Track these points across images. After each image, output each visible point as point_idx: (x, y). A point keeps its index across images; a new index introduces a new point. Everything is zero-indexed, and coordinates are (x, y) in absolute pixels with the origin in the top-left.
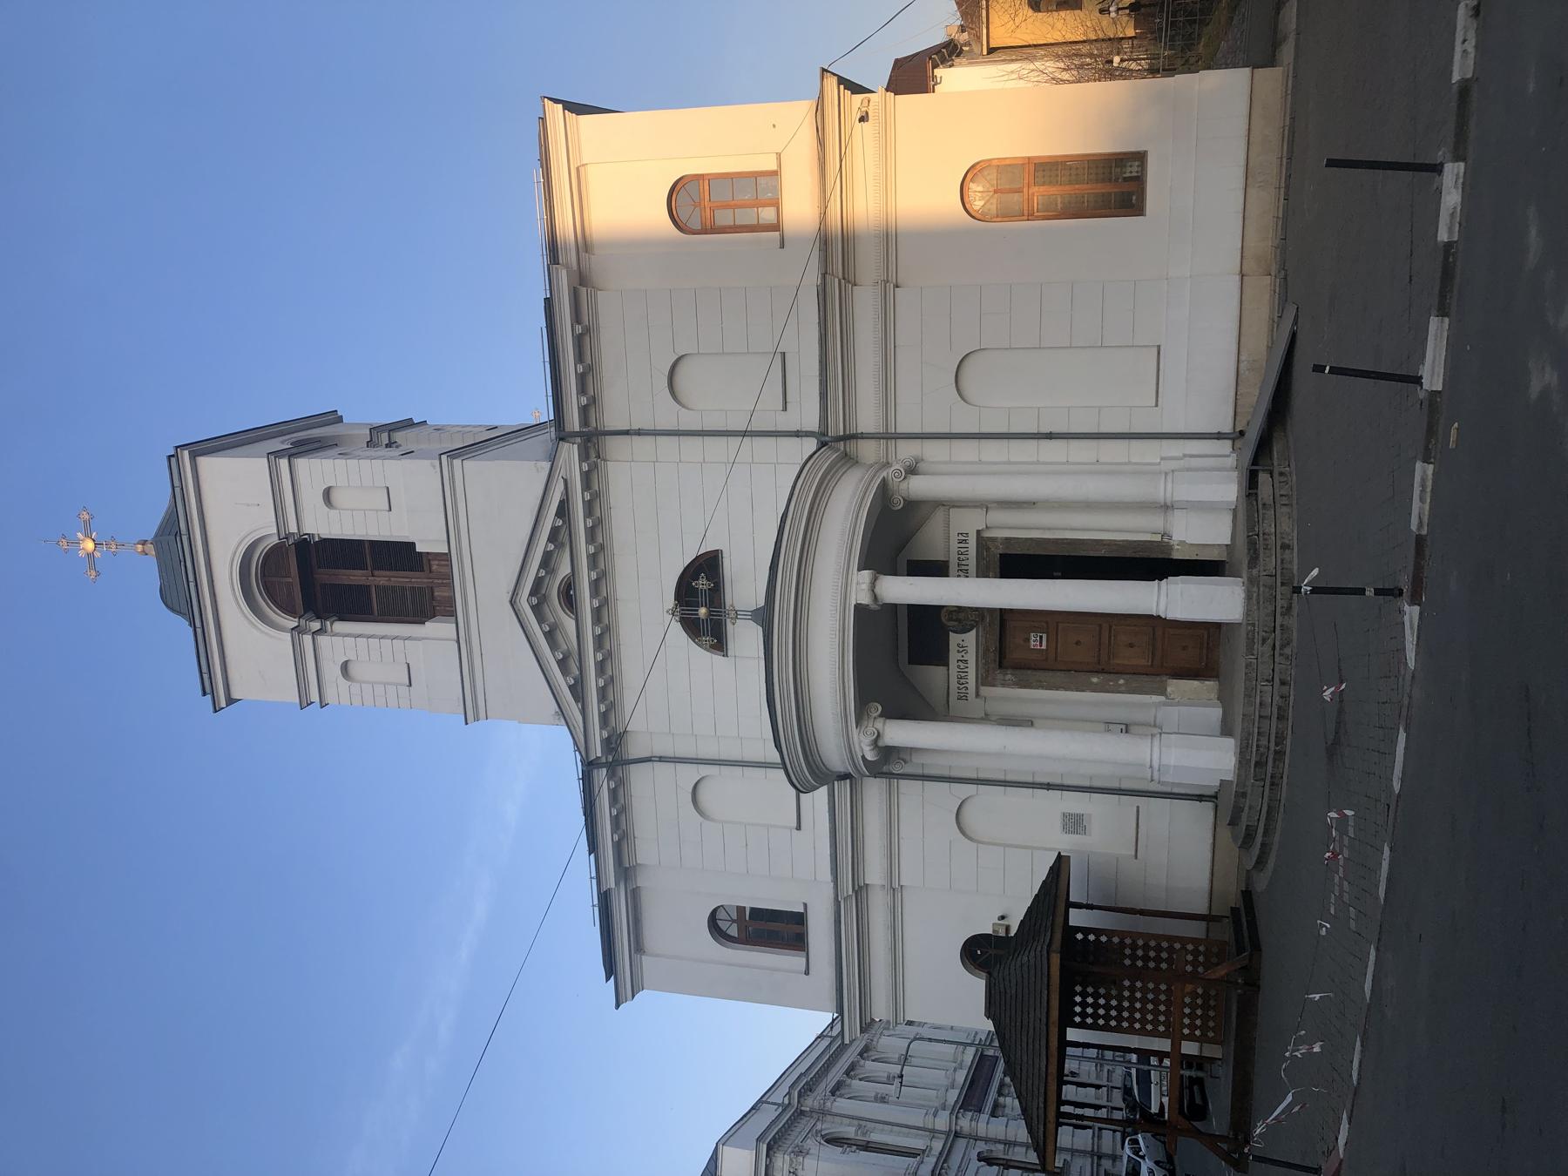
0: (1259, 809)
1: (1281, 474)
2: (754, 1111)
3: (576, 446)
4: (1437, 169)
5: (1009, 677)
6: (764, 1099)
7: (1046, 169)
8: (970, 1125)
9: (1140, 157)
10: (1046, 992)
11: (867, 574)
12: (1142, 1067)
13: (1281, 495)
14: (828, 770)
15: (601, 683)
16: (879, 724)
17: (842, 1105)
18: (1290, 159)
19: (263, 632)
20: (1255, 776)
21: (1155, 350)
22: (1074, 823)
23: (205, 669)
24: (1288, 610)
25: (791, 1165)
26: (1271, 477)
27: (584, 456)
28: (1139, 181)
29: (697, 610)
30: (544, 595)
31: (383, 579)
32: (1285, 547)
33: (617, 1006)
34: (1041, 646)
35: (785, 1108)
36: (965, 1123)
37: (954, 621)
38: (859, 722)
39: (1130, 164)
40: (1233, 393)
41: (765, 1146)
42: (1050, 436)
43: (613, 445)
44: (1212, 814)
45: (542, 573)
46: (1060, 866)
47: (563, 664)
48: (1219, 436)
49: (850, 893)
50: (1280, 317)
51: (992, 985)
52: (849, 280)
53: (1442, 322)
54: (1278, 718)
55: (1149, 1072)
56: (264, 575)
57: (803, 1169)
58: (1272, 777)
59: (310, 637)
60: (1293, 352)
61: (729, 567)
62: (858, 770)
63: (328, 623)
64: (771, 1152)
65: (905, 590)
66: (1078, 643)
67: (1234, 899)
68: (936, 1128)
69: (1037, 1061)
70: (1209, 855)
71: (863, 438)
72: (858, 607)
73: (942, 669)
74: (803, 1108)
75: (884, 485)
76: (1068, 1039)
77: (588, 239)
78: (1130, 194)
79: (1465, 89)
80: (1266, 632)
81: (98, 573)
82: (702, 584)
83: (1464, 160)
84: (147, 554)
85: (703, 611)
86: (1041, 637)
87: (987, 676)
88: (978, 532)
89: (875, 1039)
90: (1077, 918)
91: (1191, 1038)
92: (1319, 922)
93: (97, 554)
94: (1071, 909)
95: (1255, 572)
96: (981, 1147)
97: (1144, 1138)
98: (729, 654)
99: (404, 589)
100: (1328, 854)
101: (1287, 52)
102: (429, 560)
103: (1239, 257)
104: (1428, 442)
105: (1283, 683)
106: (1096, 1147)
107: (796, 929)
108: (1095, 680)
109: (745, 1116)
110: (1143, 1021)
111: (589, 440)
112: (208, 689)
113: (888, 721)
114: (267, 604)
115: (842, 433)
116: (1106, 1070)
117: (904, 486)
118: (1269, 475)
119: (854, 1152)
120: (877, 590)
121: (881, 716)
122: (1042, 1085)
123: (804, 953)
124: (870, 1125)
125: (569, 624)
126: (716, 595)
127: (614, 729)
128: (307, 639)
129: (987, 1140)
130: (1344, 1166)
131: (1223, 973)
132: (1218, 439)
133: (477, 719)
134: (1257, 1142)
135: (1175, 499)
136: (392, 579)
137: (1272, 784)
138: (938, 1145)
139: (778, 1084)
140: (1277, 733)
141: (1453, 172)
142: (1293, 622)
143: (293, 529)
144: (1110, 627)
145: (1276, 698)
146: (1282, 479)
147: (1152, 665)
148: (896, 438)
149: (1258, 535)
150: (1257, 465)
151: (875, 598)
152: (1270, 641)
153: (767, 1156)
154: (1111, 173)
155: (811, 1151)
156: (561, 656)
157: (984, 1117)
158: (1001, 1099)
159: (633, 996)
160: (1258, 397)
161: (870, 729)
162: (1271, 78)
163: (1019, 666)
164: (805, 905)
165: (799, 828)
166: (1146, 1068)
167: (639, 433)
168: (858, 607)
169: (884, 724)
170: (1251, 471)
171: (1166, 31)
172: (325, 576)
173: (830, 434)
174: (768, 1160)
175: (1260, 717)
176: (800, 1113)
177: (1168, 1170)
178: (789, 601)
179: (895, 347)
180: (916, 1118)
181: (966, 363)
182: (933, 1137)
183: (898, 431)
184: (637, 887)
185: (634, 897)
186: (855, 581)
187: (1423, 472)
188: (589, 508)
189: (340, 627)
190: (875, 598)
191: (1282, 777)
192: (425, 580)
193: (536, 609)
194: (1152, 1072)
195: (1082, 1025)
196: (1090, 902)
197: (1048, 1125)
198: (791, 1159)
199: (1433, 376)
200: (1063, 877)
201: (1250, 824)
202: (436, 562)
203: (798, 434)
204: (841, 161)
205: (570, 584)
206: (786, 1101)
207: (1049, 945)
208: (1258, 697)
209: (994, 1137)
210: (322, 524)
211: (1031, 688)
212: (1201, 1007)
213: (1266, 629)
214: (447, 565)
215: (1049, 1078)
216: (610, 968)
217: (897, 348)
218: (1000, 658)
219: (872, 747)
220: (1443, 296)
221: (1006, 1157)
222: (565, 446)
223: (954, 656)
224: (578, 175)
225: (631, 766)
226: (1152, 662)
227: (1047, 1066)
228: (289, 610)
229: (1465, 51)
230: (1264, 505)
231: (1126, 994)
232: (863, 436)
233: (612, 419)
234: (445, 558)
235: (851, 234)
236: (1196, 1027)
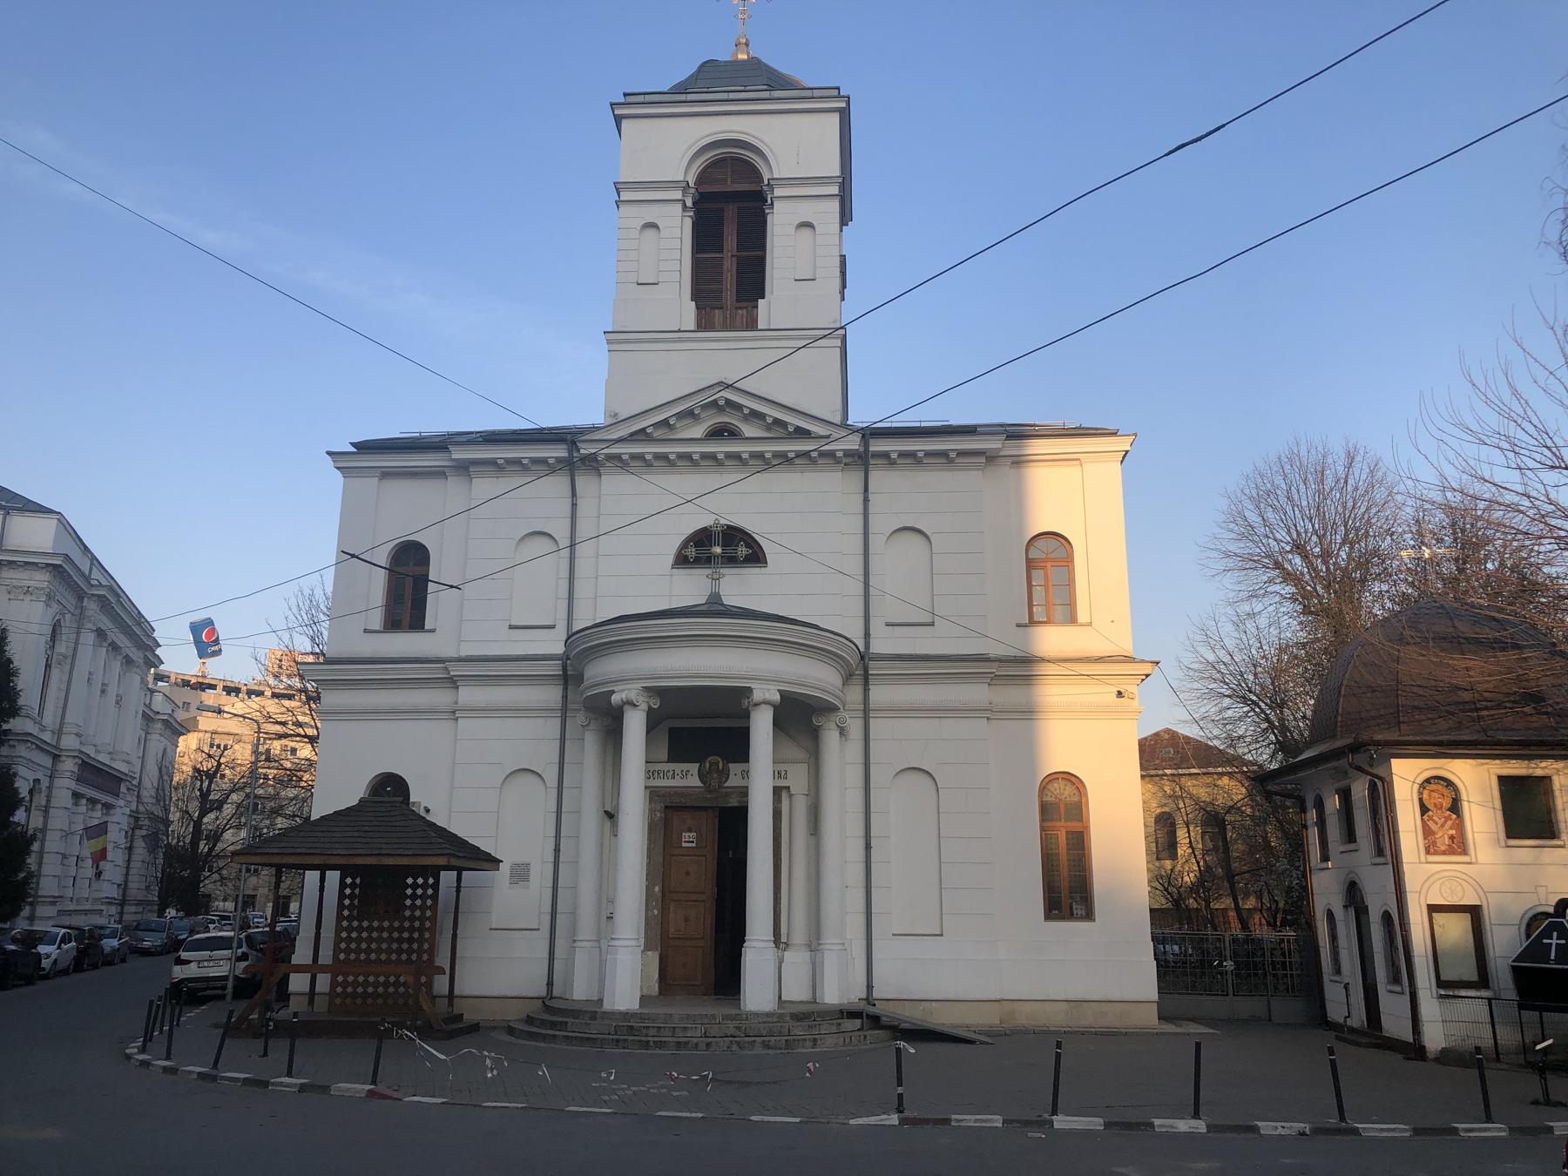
0: (587, 1031)
1: (865, 1037)
3: (857, 447)
4: (1196, 1115)
5: (658, 814)
6: (95, 562)
7: (1079, 841)
9: (1089, 915)
11: (777, 697)
12: (236, 941)
13: (851, 1037)
15: (648, 457)
16: (644, 706)
17: (88, 638)
18: (1096, 1033)
21: (938, 932)
22: (521, 874)
23: (649, 98)
24: (766, 1046)
27: (847, 453)
28: (1070, 916)
29: (718, 545)
30: (725, 410)
31: (729, 266)
33: (329, 453)
34: (685, 842)
35: (87, 579)
36: (69, 765)
37: (710, 767)
38: (646, 689)
39: (1084, 907)
40: (905, 997)
42: (868, 847)
43: (854, 478)
45: (746, 411)
47: (665, 423)
48: (870, 987)
49: (452, 673)
50: (975, 1032)
52: (995, 680)
53: (1101, 1125)
54: (678, 1042)
55: (231, 948)
56: (732, 160)
57: (9, 599)
58: (624, 1040)
59: (680, 197)
61: (752, 573)
63: (692, 214)
64: (50, 569)
65: (762, 726)
66: (688, 873)
67: (469, 1018)
70: (495, 994)
72: (750, 690)
73: (665, 757)
74: (86, 600)
75: (834, 709)
76: (327, 872)
78: (1059, 909)
79: (1255, 1129)
82: (742, 551)
83: (1208, 1131)
85: (718, 550)
86: (693, 842)
87: (659, 796)
88: (788, 788)
89: (138, 670)
90: (447, 877)
91: (334, 984)
95: (788, 1019)
96: (45, 783)
97: (72, 948)
99: (721, 282)
100: (676, 1075)
101: (1169, 1028)
102: (746, 308)
103: (1013, 998)
104: (1018, 1122)
106: (43, 899)
107: (406, 620)
108: (657, 889)
109: (80, 540)
111: (860, 457)
114: (708, 159)
115: (870, 672)
119: (46, 653)
121: (650, 708)
124: (67, 668)
125: (698, 431)
126: (731, 560)
128: (678, 195)
129: (50, 788)
131: (425, 1008)
132: (868, 987)
133: (609, 342)
134: (397, 1033)
135: (826, 954)
136: (729, 274)
137: (617, 1041)
138: (47, 737)
139: (106, 575)
140: (665, 1042)
141: (1200, 1126)
142: (758, 1050)
143: (778, 192)
145: (695, 1040)
146: (862, 1037)
148: (865, 718)
149: (814, 1020)
150: (867, 1018)
151: (757, 705)
152: (738, 1033)
153: (48, 565)
154: (1076, 893)
156: (672, 423)
157: (73, 785)
158: (99, 806)
159: (338, 468)
161: (641, 699)
162: (1149, 1017)
163: (667, 823)
164: (433, 631)
165: (511, 627)
167: (866, 500)
168: (750, 690)
171: (1178, 934)
172: (731, 212)
174: (22, 564)
175: (674, 1028)
179: (940, 717)
181: (931, 782)
182: (53, 733)
183: (871, 720)
185: (438, 474)
186: (769, 687)
187: (997, 1121)
189: (688, 223)
191: (624, 1048)
193: (714, 403)
194: (231, 951)
195: (343, 885)
196: (462, 889)
197: (279, 857)
199: (1061, 1122)
200: (486, 865)
201: (569, 1025)
203: (867, 635)
204: (1088, 675)
205: (736, 435)
207: (454, 855)
208: (690, 1026)
209: (53, 795)
210: (781, 221)
213: (747, 1030)
215: (326, 857)
216: (364, 447)
218: (674, 807)
219: (625, 700)
220: (1117, 1124)
221: (33, 808)
222: (857, 438)
223: (678, 767)
228: (702, 178)
229: (1277, 1128)
230: (840, 1024)
232: (866, 691)
233: (876, 477)
234: (751, 324)
235: (1034, 682)
236: (345, 988)
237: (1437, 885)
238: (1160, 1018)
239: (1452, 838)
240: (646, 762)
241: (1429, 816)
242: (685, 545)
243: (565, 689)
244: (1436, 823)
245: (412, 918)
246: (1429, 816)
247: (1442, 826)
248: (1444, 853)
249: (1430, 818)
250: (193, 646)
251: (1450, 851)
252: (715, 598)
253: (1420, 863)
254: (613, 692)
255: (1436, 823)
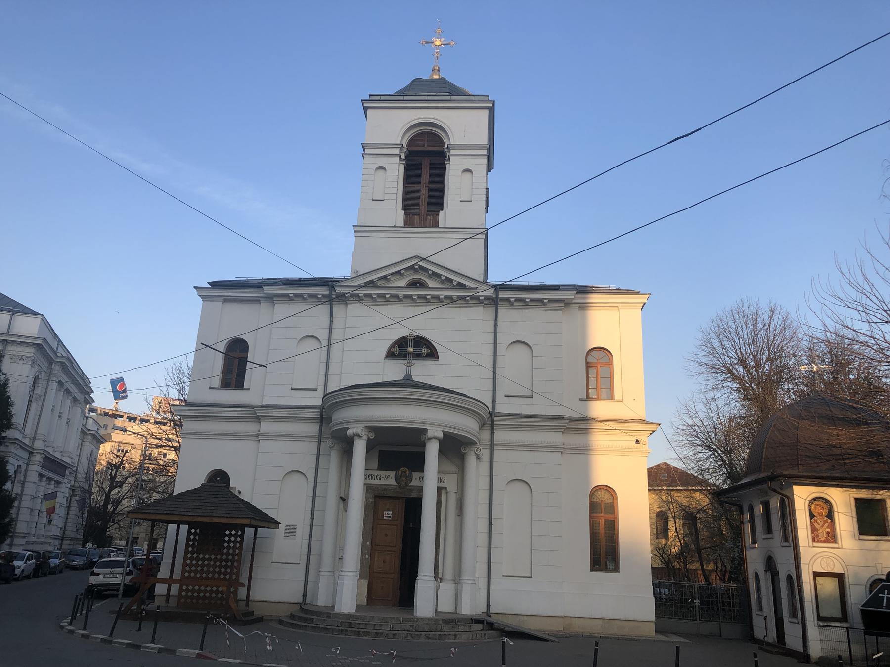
1: (485, 635)
2: (54, 335)
5: (371, 500)
6: (60, 343)
8: (35, 461)
9: (616, 569)
10: (229, 516)
11: (441, 435)
14: (334, 411)
16: (365, 437)
17: (54, 386)
19: (402, 129)
20: (343, 622)
22: (291, 531)
25: (27, 357)
26: (481, 630)
27: (486, 298)
28: (605, 569)
32: (455, 636)
33: (195, 287)
34: (385, 517)
35: (55, 353)
36: (38, 458)
37: (401, 474)
41: (40, 343)
42: (490, 524)
43: (490, 312)
44: (296, 602)
45: (430, 272)
46: (275, 523)
47: (385, 277)
48: (488, 606)
49: (258, 414)
51: (221, 488)
52: (566, 430)
57: (11, 362)
58: (346, 630)
59: (398, 153)
60: (541, 640)
61: (430, 363)
62: (334, 426)
63: (404, 162)
64: (35, 346)
65: (432, 452)
66: (386, 535)
68: (36, 441)
69: (190, 510)
70: (273, 600)
71: (492, 433)
72: (426, 430)
77: (586, 308)
80: (416, 627)
81: (423, 45)
82: (425, 351)
84: (433, 71)
85: (411, 350)
86: (390, 517)
90: (249, 531)
91: (181, 590)
92: (339, 648)
93: (433, 46)
94: (176, 525)
96: (24, 467)
98: (386, 360)
101: (662, 638)
105: (394, 635)
108: (368, 543)
110: (191, 565)
111: (493, 300)
112: (372, 98)
113: (366, 442)
115: (495, 423)
116: (50, 541)
117: (472, 453)
118: (481, 629)
119: (29, 393)
120: (434, 440)
121: (369, 438)
122: (177, 513)
123: (219, 387)
125: (403, 283)
126: (418, 356)
127: (348, 300)
129: (26, 470)
130: (215, 661)
132: (487, 605)
134: (216, 620)
135: (464, 585)
138: (26, 441)
140: (369, 632)
142: (422, 640)
143: (453, 152)
144: (394, 551)
147: (374, 572)
148: (491, 449)
151: (430, 439)
155: (33, 369)
157: (39, 469)
159: (200, 296)
160: (512, 623)
161: (364, 433)
162: (649, 631)
164: (248, 389)
165: (292, 389)
166: (125, 566)
167: (496, 325)
168: (426, 430)
169: (365, 440)
170: (484, 620)
172: (426, 162)
173: (495, 417)
174: (31, 344)
175: (375, 624)
176: (51, 362)
177: (19, 577)
178: (421, 396)
180: (42, 430)
182: (31, 439)
184: (260, 303)
185: (256, 301)
188: (463, 298)
189: (402, 167)
190: (430, 439)
191: (346, 635)
192: (423, 212)
195: (189, 533)
198: (30, 357)
202: (432, 218)
203: (494, 401)
204: (620, 430)
206: (59, 355)
207: (254, 519)
210: (454, 168)
211: (365, 511)
212: (198, 596)
214: (430, 226)
216: (215, 285)
217: (533, 452)
219: (355, 433)
222: (492, 290)
224: (614, 306)
225: (329, 306)
226: (376, 572)
227: (188, 515)
228: (411, 143)
231: (195, 556)
233: (502, 312)
234: (435, 224)
237: (819, 560)
238: (656, 632)
239: (828, 533)
240: (365, 470)
241: (814, 520)
242: (392, 346)
243: (321, 426)
244: (819, 524)
245: (228, 554)
246: (814, 520)
247: (822, 526)
248: (823, 542)
249: (816, 521)
250: (112, 393)
251: (827, 541)
252: (408, 377)
253: (809, 547)
254: (348, 428)
255: (819, 524)
